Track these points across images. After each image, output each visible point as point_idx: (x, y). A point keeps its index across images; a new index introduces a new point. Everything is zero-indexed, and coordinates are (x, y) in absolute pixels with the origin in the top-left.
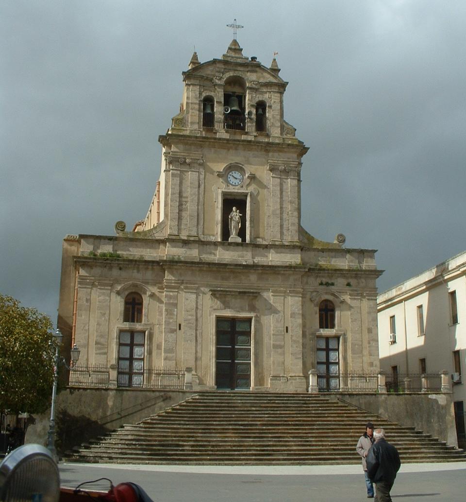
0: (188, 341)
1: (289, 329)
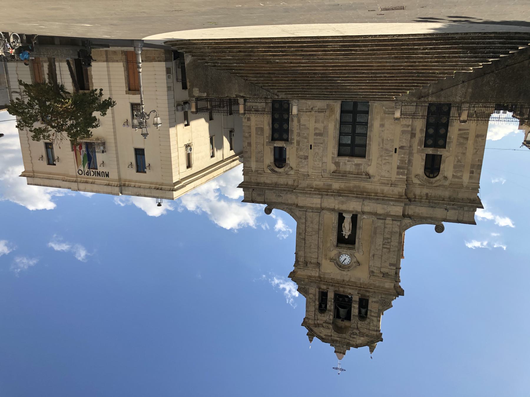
0: (390, 139)
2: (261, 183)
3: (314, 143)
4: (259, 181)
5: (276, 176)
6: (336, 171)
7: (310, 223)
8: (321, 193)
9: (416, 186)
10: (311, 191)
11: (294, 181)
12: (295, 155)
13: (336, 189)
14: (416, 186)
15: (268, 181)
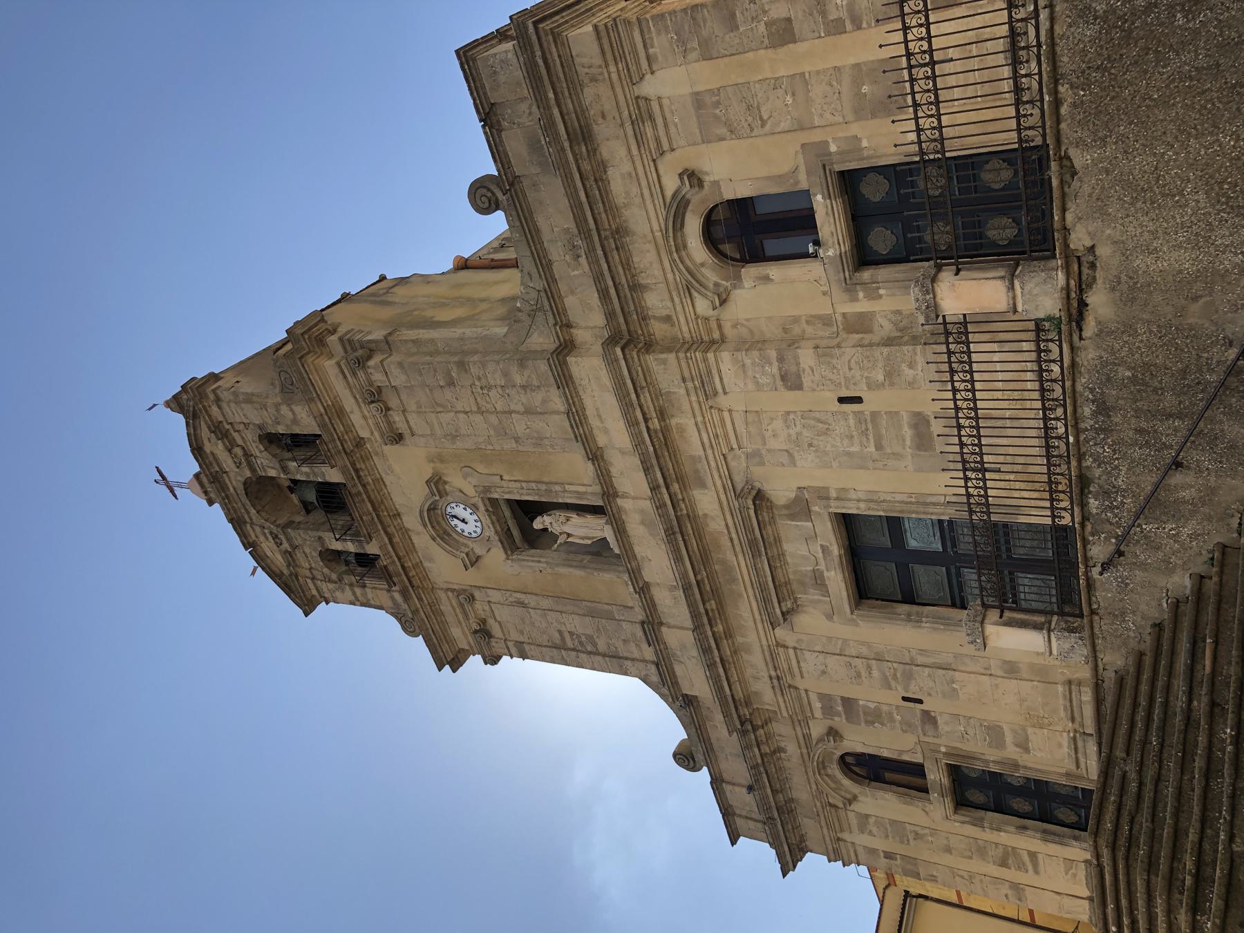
0: (955, 690)
1: (845, 393)
2: (593, 152)
3: (874, 415)
4: (602, 130)
5: (656, 227)
6: (771, 507)
7: (524, 401)
8: (654, 462)
9: (798, 729)
10: (646, 420)
11: (668, 319)
12: (795, 313)
13: (692, 505)
14: (798, 729)
15: (618, 185)
